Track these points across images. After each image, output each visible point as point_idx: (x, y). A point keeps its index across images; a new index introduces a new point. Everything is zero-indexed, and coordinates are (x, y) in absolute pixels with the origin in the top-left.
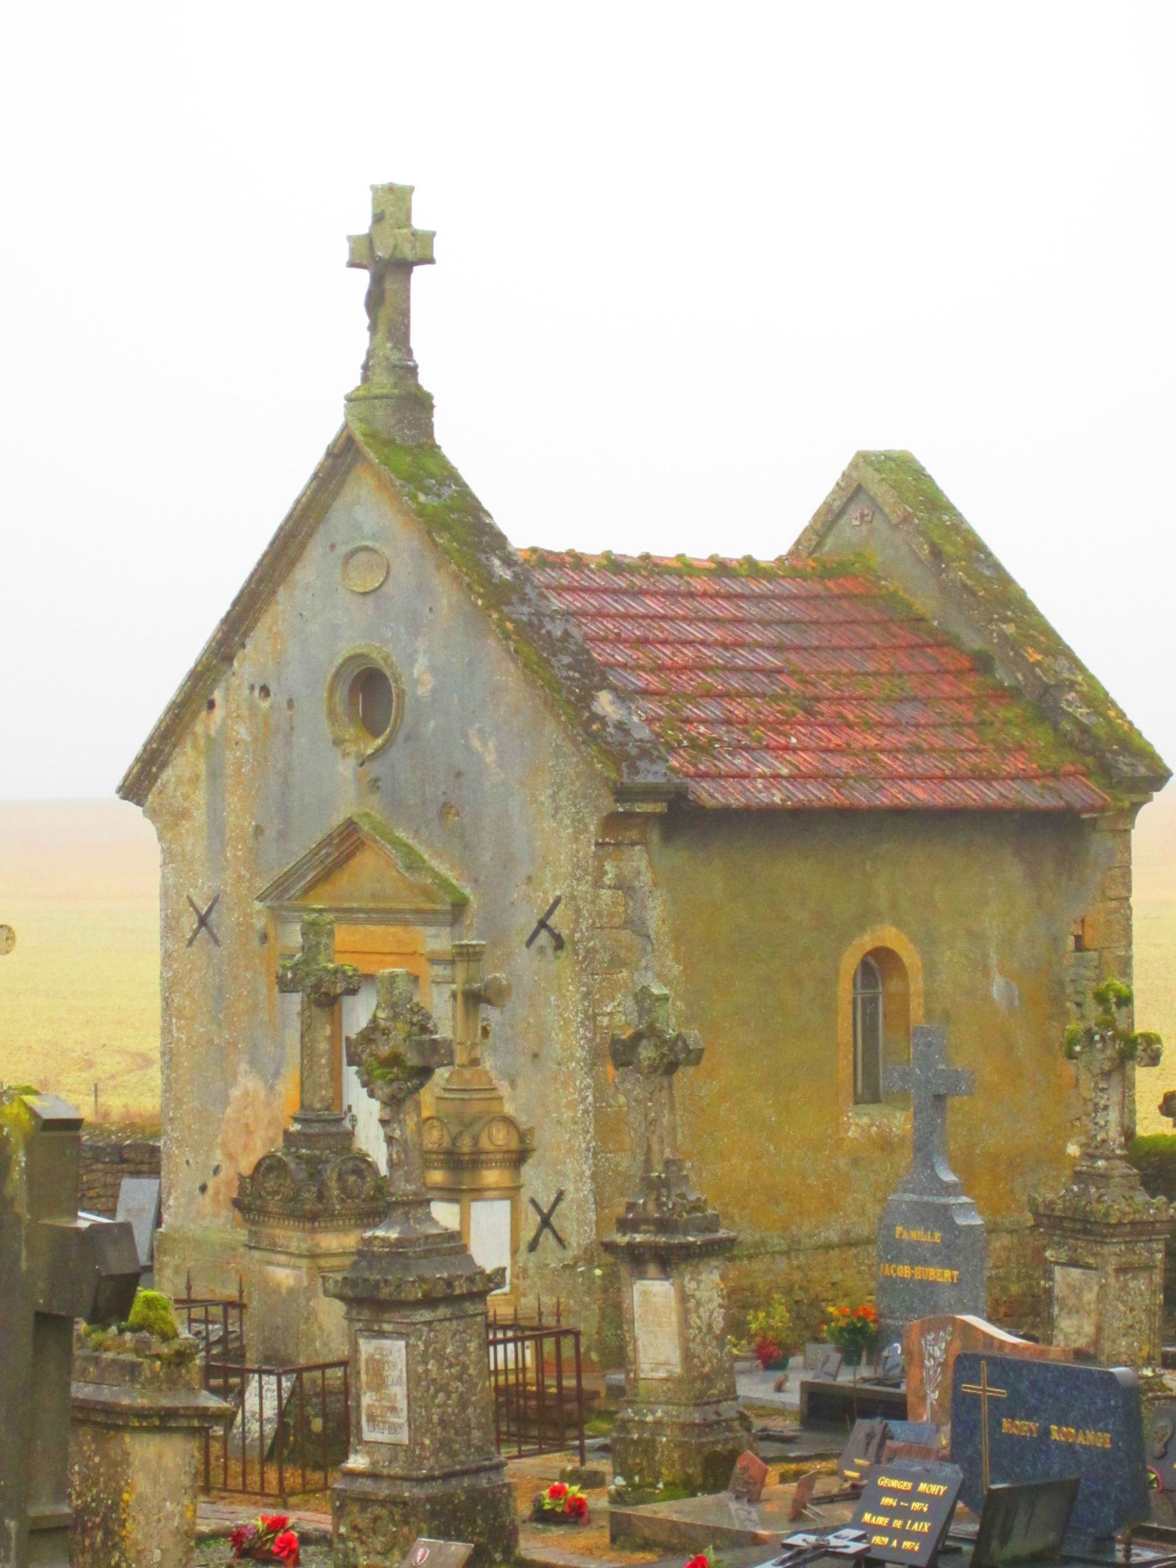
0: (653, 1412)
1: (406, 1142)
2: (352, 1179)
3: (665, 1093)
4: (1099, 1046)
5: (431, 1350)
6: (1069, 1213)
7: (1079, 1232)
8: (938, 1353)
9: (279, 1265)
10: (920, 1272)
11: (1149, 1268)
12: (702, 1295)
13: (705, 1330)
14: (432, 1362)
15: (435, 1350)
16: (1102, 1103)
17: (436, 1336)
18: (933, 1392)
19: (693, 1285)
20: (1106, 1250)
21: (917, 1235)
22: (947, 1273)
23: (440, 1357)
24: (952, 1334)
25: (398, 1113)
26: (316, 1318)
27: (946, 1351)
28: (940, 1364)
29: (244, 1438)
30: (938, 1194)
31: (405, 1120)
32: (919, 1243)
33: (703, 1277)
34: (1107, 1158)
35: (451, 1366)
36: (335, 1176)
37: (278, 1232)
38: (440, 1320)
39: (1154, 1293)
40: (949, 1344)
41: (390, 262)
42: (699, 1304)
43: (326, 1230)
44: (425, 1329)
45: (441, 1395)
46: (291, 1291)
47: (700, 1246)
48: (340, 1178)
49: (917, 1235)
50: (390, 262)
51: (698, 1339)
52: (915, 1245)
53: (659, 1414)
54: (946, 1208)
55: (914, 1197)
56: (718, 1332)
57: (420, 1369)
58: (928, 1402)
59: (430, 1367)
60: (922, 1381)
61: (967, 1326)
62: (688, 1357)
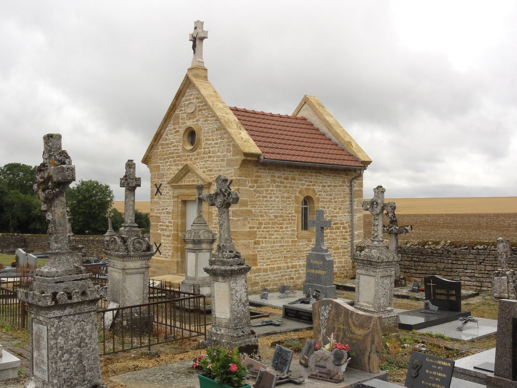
0: (220, 330)
1: (55, 222)
2: (138, 245)
3: (225, 214)
4: (375, 206)
5: (60, 332)
6: (365, 259)
7: (369, 264)
8: (326, 314)
9: (116, 272)
10: (318, 272)
11: (390, 276)
12: (238, 288)
13: (239, 301)
14: (60, 338)
15: (63, 332)
16: (377, 224)
17: (64, 324)
18: (323, 329)
19: (234, 284)
20: (378, 271)
21: (316, 262)
22: (324, 272)
23: (65, 335)
24: (331, 307)
25: (51, 207)
26: (125, 289)
27: (329, 314)
28: (326, 319)
29: (104, 325)
30: (322, 252)
31: (54, 211)
32: (317, 264)
33: (238, 282)
34: (378, 241)
35: (73, 339)
36: (131, 244)
37: (115, 261)
38: (66, 316)
39: (391, 283)
40: (330, 311)
41: (197, 40)
42: (236, 292)
43: (129, 261)
44: (56, 321)
45: (66, 356)
46: (118, 280)
47: (236, 270)
48: (133, 245)
49: (316, 262)
50: (197, 40)
51: (236, 305)
52: (316, 265)
53: (222, 331)
54: (324, 255)
55: (316, 253)
56: (244, 302)
57: (52, 342)
58: (322, 333)
59: (59, 341)
60: (319, 324)
61: (337, 305)
62: (232, 311)
